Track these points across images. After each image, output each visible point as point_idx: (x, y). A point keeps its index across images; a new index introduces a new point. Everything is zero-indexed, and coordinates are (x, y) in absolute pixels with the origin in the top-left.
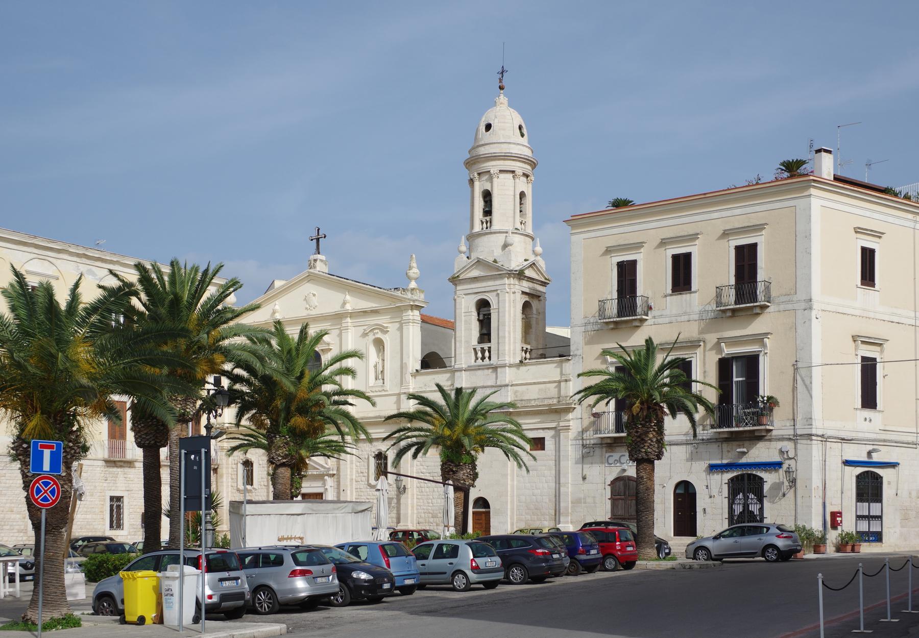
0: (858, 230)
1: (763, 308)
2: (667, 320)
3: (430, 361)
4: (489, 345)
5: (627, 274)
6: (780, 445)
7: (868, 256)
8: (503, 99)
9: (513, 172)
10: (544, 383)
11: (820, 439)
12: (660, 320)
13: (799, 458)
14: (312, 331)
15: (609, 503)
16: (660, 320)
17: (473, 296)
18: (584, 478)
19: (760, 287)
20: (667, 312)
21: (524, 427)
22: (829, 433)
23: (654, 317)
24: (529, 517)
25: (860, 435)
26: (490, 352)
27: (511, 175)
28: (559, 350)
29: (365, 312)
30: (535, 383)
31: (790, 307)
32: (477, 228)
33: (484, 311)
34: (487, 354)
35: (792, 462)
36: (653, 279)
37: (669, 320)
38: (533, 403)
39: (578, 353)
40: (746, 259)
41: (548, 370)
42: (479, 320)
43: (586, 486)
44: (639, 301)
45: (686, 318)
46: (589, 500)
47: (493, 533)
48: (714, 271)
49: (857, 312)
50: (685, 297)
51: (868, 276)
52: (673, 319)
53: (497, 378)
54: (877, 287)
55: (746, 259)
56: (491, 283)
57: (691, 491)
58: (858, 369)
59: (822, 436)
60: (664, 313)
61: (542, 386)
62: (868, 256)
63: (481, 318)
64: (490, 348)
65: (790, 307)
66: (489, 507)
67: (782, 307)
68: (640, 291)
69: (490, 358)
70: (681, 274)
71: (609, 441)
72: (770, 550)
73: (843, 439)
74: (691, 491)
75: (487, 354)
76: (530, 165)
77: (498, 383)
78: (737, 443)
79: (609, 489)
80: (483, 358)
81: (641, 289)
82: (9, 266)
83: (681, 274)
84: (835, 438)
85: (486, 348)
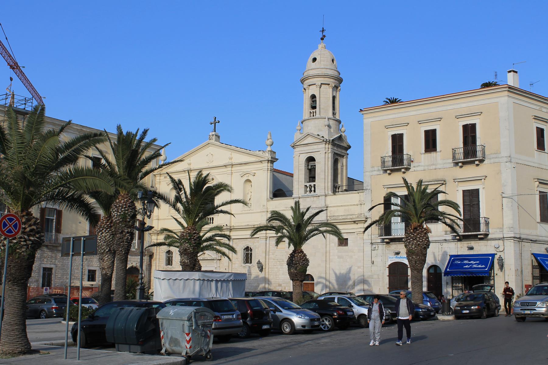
0: (536, 118)
1: (481, 161)
2: (422, 168)
3: (279, 192)
4: (314, 183)
5: (397, 141)
6: (494, 243)
7: (540, 133)
8: (321, 46)
10: (348, 206)
11: (518, 240)
12: (419, 169)
13: (505, 251)
14: (205, 173)
15: (287, 266)
16: (419, 169)
19: (479, 149)
20: (422, 164)
21: (342, 231)
22: (523, 237)
23: (414, 167)
25: (540, 238)
26: (315, 188)
28: (353, 185)
30: (342, 206)
31: (497, 160)
32: (306, 115)
33: (311, 163)
34: (313, 189)
35: (501, 254)
36: (413, 145)
37: (425, 168)
38: (341, 218)
39: (369, 188)
40: (469, 132)
41: (353, 197)
42: (308, 169)
44: (405, 157)
45: (434, 167)
46: (375, 277)
47: (397, 325)
48: (451, 140)
49: (536, 165)
50: (433, 154)
51: (541, 146)
52: (426, 168)
54: (546, 151)
55: (469, 132)
56: (315, 147)
57: (438, 272)
58: (537, 197)
59: (520, 238)
60: (420, 164)
61: (346, 208)
62: (540, 133)
63: (310, 168)
64: (315, 185)
65: (497, 160)
67: (492, 161)
68: (405, 152)
69: (315, 191)
70: (430, 141)
71: (387, 240)
73: (531, 240)
74: (438, 272)
75: (313, 189)
79: (387, 270)
80: (311, 191)
81: (407, 150)
83: (430, 141)
84: (527, 239)
85: (312, 185)
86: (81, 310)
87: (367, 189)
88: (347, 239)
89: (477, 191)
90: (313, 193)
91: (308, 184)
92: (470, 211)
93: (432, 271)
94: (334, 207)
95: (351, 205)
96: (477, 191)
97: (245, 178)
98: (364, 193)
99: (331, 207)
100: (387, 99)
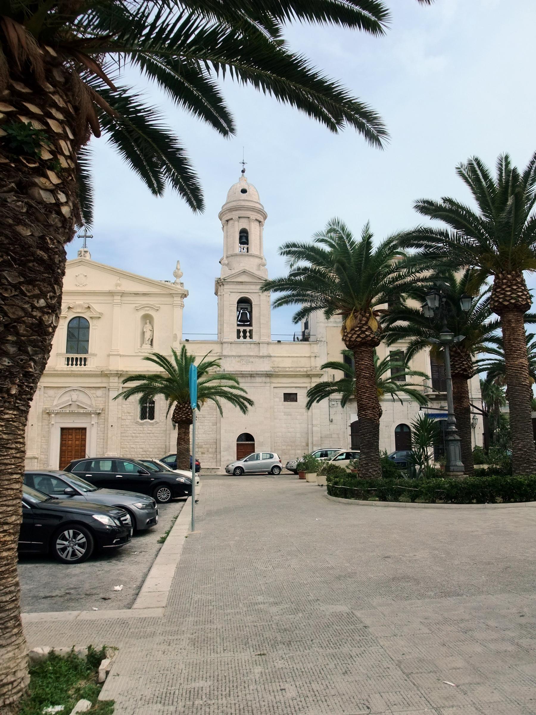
4: (251, 328)
9: (249, 218)
10: (297, 357)
15: (350, 438)
17: (239, 294)
18: (331, 421)
24: (284, 447)
27: (247, 219)
29: (131, 293)
30: (289, 357)
38: (287, 369)
39: (323, 340)
43: (332, 427)
53: (259, 351)
61: (295, 359)
66: (254, 441)
72: (69, 533)
76: (263, 216)
77: (261, 354)
78: (437, 402)
79: (349, 429)
82: (365, 223)
86: (78, 458)
87: (321, 341)
88: (296, 394)
89: (83, 430)
90: (248, 339)
91: (242, 329)
92: (438, 371)
93: (399, 430)
94: (278, 357)
95: (301, 357)
96: (83, 430)
97: (142, 313)
98: (319, 345)
99: (275, 357)
100: (427, 208)
